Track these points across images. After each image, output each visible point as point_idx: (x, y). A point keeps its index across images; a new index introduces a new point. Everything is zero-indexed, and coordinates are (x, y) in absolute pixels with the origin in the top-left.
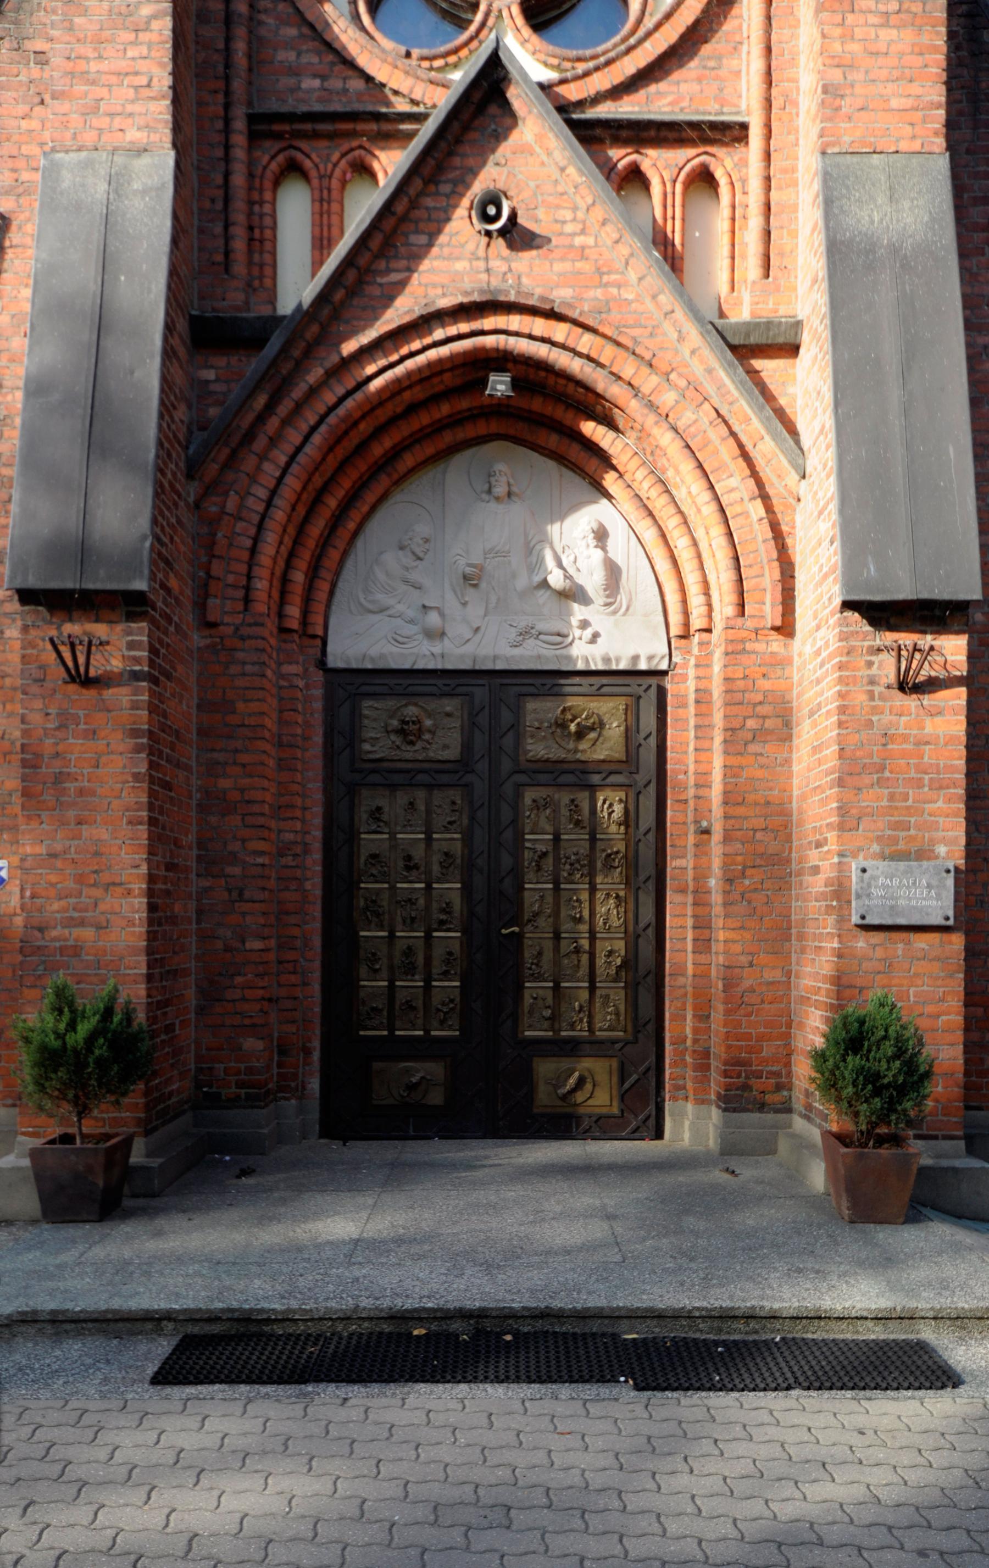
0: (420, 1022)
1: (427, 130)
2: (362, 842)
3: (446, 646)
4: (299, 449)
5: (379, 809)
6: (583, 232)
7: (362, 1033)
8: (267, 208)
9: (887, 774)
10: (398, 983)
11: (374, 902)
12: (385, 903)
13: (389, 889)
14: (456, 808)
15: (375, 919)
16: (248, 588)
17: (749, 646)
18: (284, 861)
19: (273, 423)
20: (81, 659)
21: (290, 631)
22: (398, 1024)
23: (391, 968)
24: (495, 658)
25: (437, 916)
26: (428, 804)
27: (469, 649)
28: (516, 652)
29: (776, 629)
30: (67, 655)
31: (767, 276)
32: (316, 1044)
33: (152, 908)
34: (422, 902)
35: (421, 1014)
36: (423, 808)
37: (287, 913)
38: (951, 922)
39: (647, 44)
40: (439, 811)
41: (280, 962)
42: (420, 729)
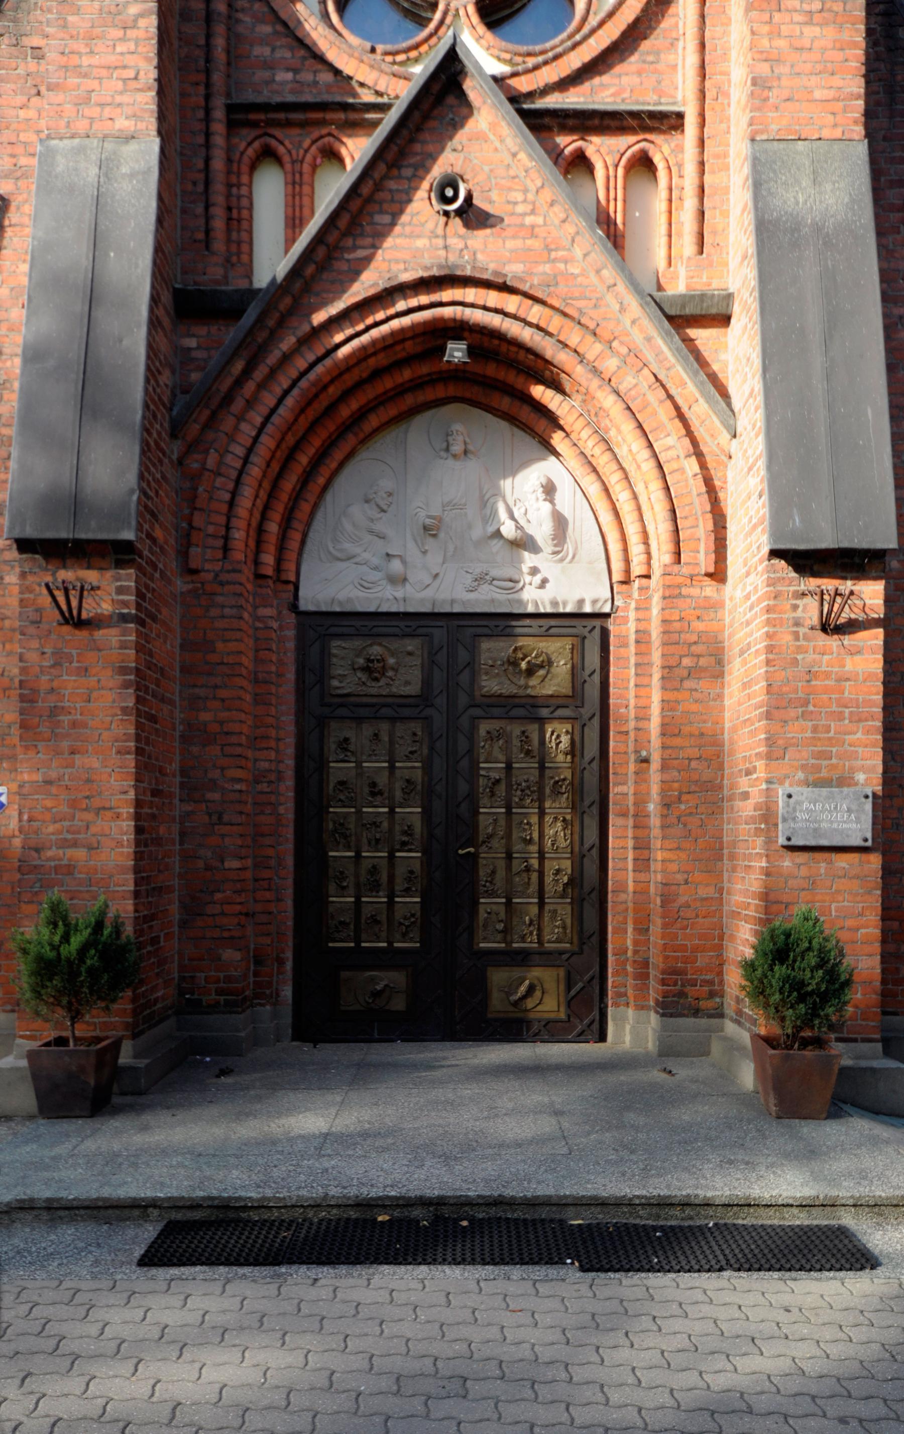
0: (384, 934)
1: (390, 119)
2: (331, 770)
3: (408, 590)
4: (273, 411)
5: (346, 740)
6: (533, 212)
7: (331, 945)
8: (244, 190)
9: (811, 708)
10: (363, 899)
11: (342, 825)
12: (352, 826)
13: (356, 813)
14: (417, 739)
15: (343, 841)
16: (226, 538)
17: (684, 591)
18: (259, 787)
19: (250, 387)
20: (74, 603)
21: (265, 577)
22: (364, 936)
23: (358, 885)
24: (453, 601)
25: (399, 837)
26: (391, 735)
27: (428, 593)
28: (472, 596)
29: (709, 575)
30: (61, 599)
31: (701, 252)
32: (289, 954)
33: (139, 830)
34: (385, 825)
35: (385, 927)
36: (386, 739)
37: (263, 835)
38: (869, 843)
39: (592, 41)
40: (401, 742)
41: (256, 880)
42: (384, 667)
